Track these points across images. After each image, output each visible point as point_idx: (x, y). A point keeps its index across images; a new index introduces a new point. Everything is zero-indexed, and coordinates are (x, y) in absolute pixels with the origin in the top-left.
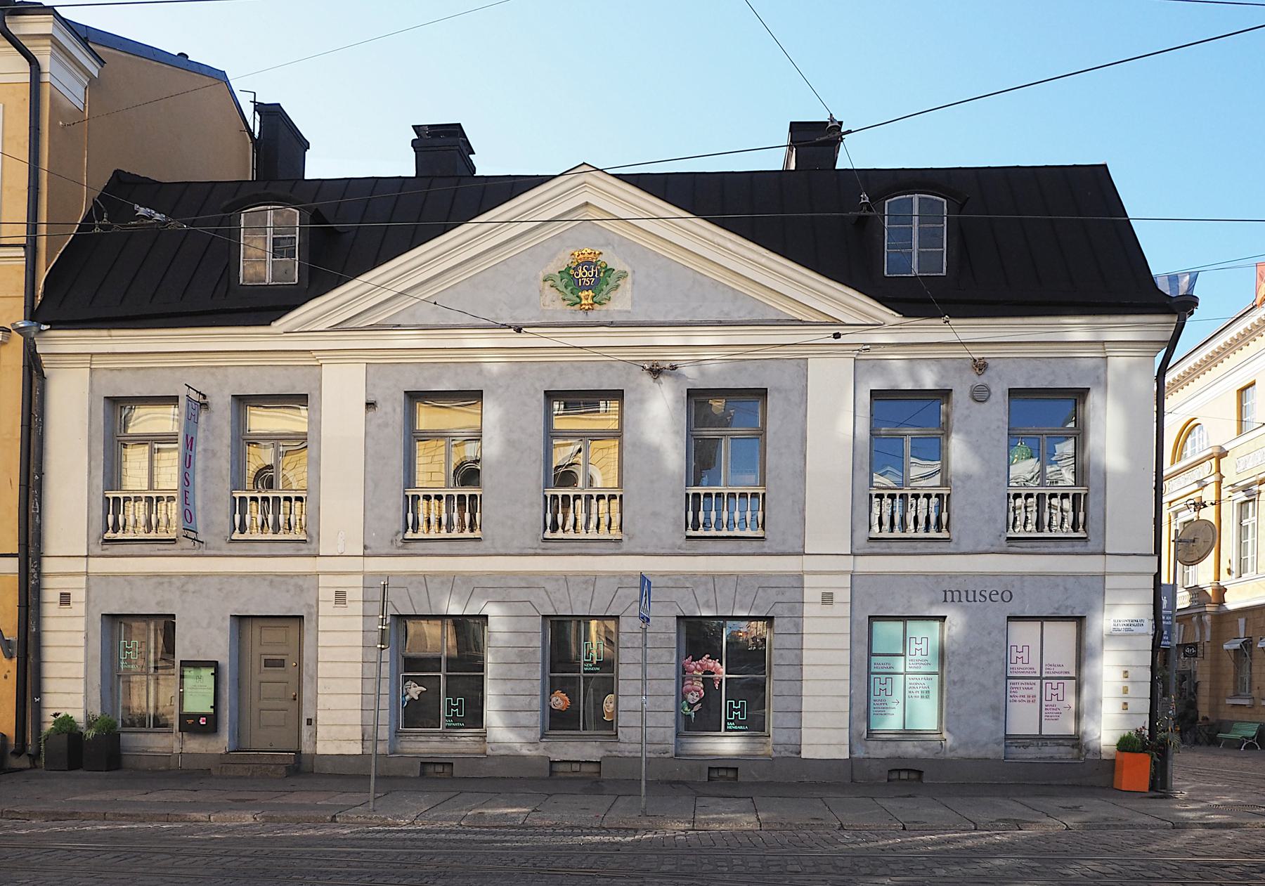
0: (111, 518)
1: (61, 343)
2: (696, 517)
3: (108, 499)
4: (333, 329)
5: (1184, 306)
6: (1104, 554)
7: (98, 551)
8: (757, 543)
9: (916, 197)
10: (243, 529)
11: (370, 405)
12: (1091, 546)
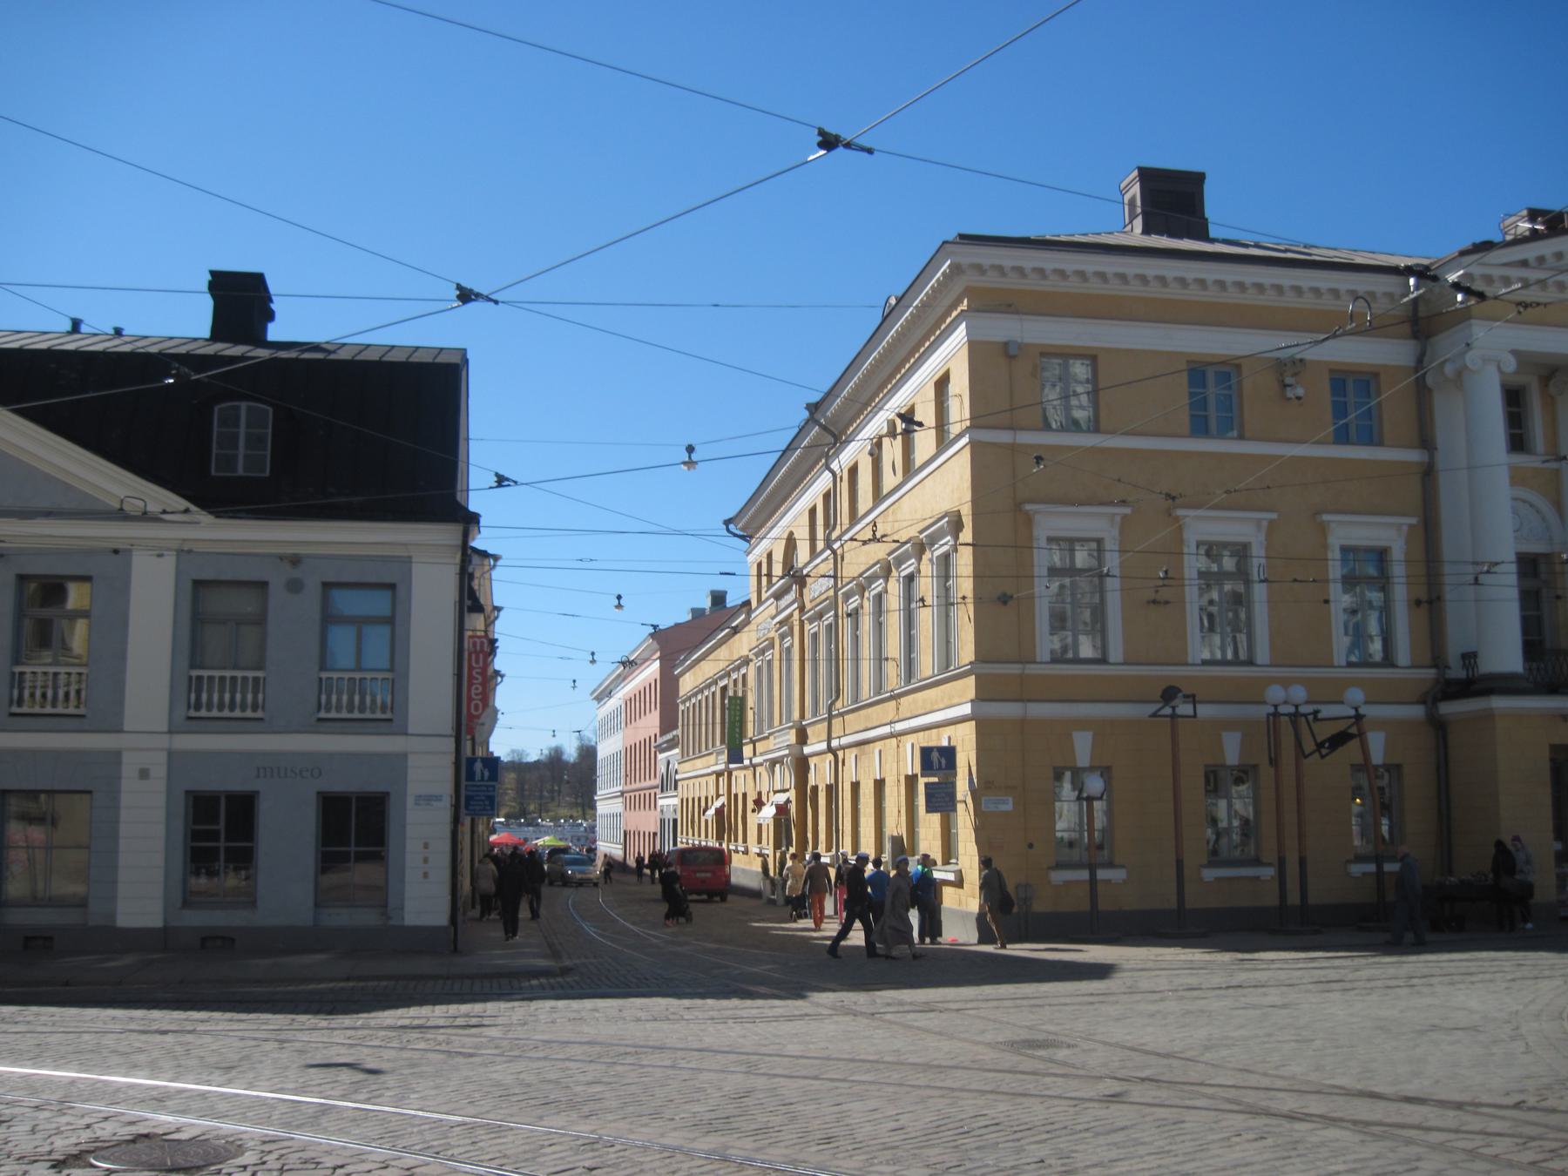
0: (324, 698)
2: (198, 698)
3: (13, 674)
8: (77, 722)
9: (244, 405)
10: (20, 702)
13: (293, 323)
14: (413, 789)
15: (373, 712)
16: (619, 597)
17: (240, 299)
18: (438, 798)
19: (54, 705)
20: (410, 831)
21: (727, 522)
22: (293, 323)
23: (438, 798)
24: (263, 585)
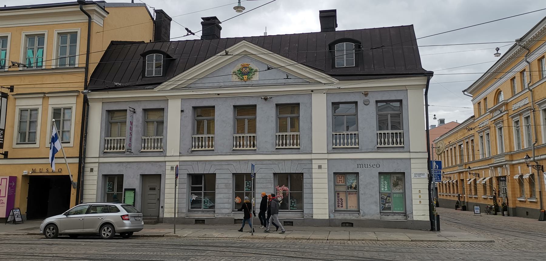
1: (93, 96)
4: (172, 89)
5: (431, 74)
6: (410, 152)
7: (102, 155)
9: (155, 54)
11: (182, 111)
12: (405, 149)
13: (343, 24)
14: (413, 171)
15: (344, 145)
16: (435, 115)
17: (328, 18)
18: (423, 174)
19: (198, 148)
20: (413, 186)
21: (464, 91)
22: (343, 24)
23: (423, 174)
24: (356, 103)
